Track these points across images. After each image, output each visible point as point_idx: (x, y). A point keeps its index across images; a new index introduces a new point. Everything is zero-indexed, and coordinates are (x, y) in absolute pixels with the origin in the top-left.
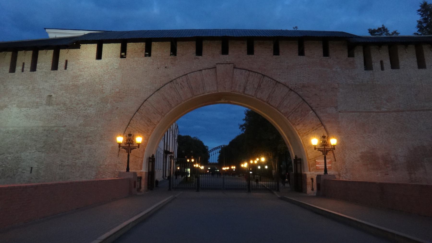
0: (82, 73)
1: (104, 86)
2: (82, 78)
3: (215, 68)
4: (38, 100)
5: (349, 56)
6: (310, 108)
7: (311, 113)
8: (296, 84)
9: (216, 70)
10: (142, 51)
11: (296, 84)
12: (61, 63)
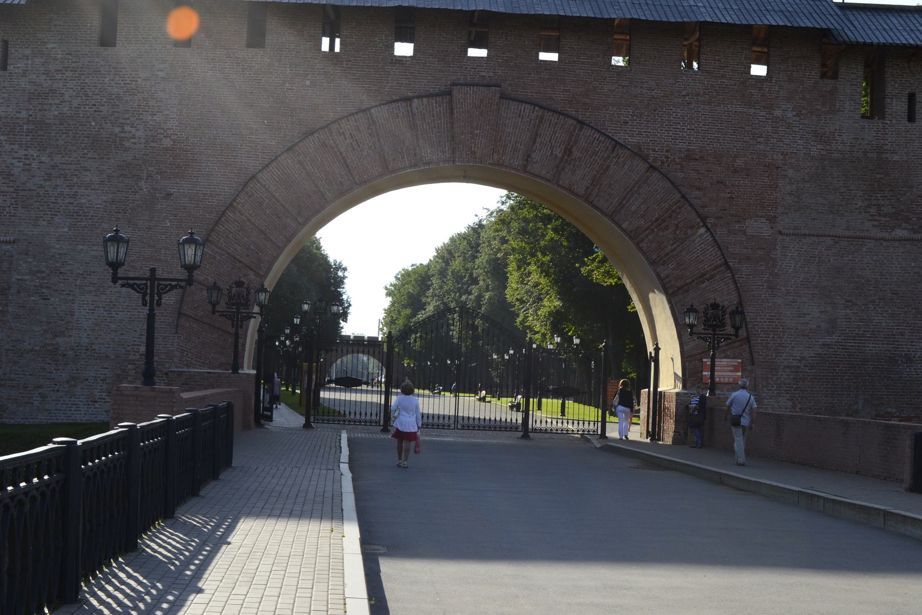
0: (55, 86)
2: (57, 101)
3: (450, 93)
5: (823, 75)
6: (698, 220)
7: (701, 235)
8: (667, 151)
9: (451, 102)
11: (667, 151)
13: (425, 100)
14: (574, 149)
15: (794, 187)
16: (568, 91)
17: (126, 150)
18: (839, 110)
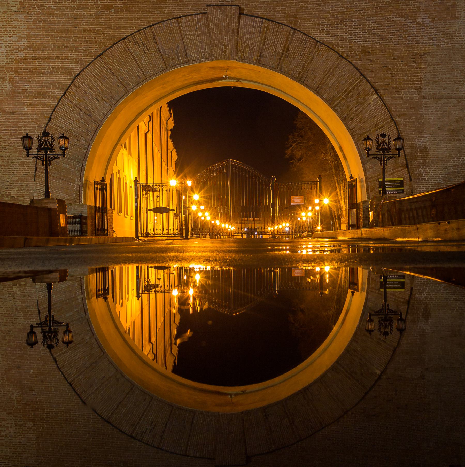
6: (372, 90)
7: (374, 100)
8: (351, 47)
9: (207, 19)
11: (351, 47)
13: (190, 17)
14: (290, 47)
15: (432, 68)
16: (284, 9)
18: (458, 18)
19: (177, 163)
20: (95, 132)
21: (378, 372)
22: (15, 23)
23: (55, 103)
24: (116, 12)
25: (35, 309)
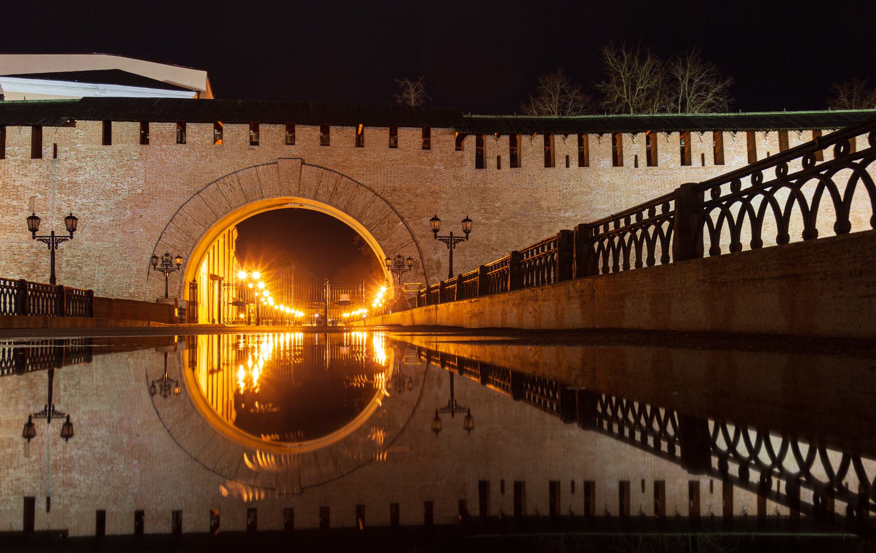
1: (119, 184)
4: (15, 203)
10: (645, 456)
12: (47, 150)
17: (119, 195)
19: (238, 242)
20: (193, 247)
21: (402, 425)
22: (135, 168)
23: (164, 226)
24: (211, 161)
25: (144, 375)
